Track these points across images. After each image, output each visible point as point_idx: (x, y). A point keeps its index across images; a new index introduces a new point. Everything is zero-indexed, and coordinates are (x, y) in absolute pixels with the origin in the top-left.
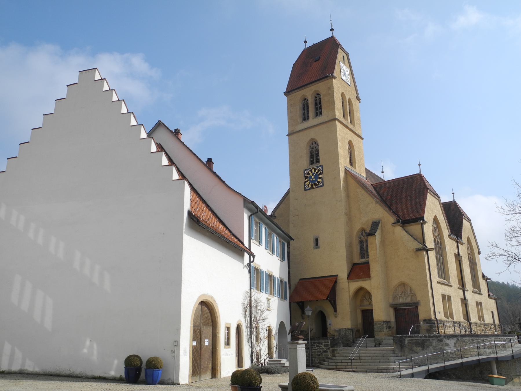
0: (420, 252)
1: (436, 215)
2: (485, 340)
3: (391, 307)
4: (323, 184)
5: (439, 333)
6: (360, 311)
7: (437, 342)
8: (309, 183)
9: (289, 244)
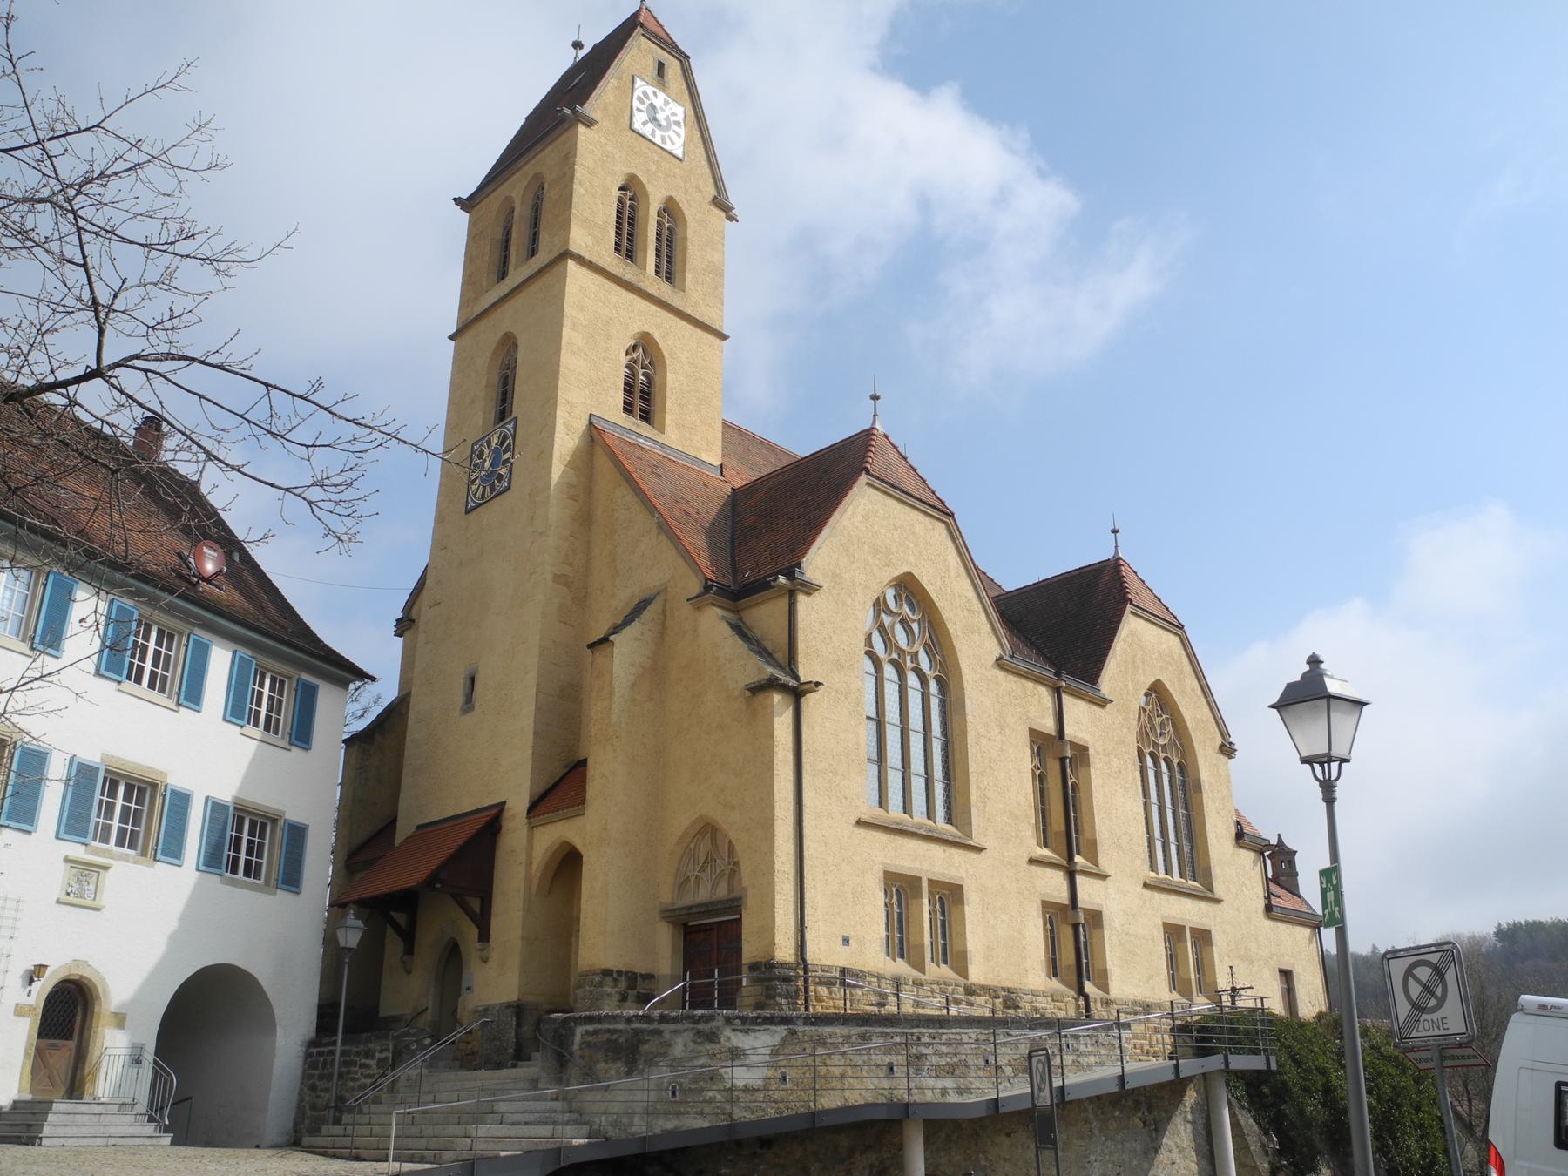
0: (760, 697)
2: (925, 1040)
3: (664, 918)
4: (510, 484)
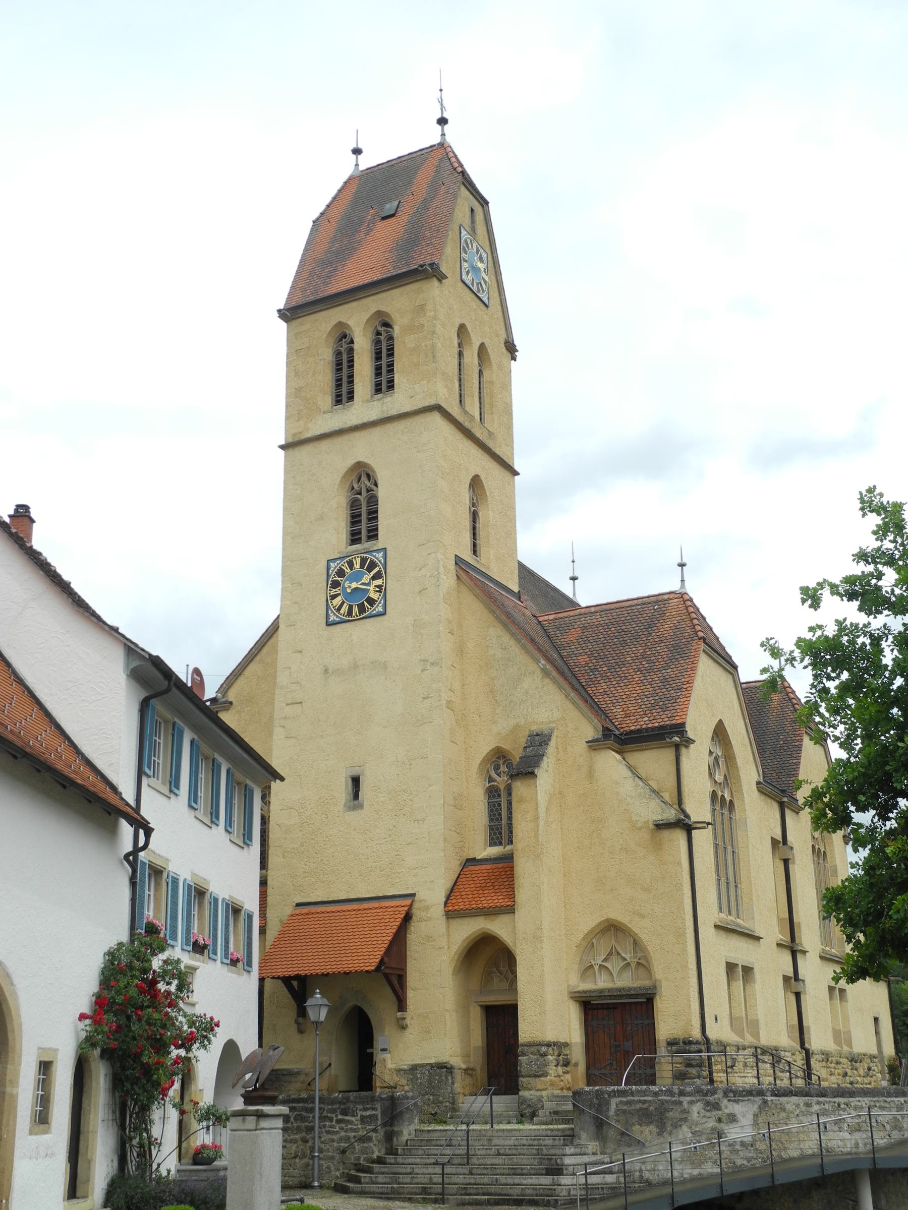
1: (721, 720)
2: (842, 1106)
5: (712, 1081)
6: (479, 1009)
7: (703, 1111)
8: (343, 603)
9: (270, 793)
